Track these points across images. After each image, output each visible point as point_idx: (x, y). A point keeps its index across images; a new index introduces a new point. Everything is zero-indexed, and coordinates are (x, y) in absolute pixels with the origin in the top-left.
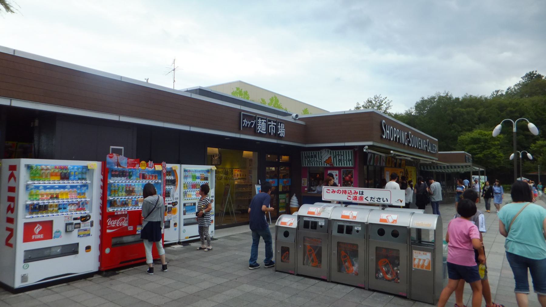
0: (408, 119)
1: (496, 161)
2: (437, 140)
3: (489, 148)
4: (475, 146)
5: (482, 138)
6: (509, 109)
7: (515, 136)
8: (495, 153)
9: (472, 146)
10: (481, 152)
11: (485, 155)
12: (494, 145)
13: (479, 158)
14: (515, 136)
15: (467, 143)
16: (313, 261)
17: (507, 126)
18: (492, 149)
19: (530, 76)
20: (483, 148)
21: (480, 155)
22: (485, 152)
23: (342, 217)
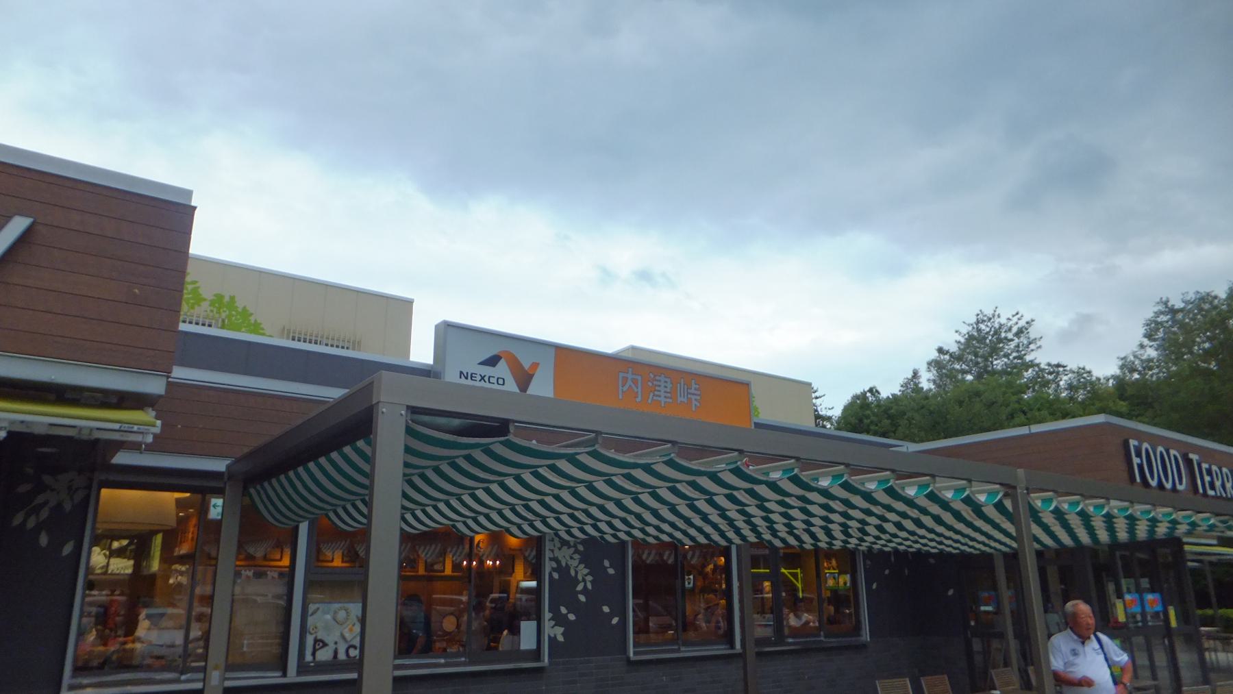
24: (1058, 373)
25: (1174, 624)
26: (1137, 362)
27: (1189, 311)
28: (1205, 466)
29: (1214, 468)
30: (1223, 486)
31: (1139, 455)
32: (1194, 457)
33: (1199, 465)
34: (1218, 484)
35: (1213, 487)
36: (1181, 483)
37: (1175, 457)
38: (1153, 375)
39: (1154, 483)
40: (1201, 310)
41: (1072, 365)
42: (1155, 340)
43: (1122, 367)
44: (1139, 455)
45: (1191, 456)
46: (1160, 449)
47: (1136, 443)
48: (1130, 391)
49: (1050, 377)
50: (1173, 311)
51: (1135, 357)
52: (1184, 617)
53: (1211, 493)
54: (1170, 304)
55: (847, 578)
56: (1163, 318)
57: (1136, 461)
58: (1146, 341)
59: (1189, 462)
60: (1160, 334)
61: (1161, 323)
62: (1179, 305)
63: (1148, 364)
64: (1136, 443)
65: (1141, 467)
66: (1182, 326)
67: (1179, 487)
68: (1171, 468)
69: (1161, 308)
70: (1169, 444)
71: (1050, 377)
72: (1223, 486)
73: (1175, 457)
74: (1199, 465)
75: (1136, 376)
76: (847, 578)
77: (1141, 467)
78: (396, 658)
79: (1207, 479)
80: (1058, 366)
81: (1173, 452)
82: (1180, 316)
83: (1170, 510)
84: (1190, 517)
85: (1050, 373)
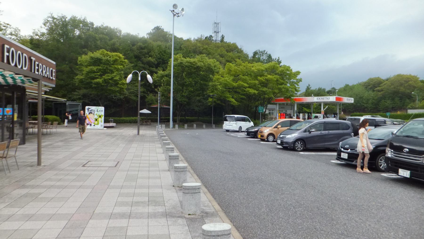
0: (34, 44)
1: (118, 89)
2: (54, 63)
3: (112, 72)
4: (95, 68)
5: (104, 58)
6: (139, 44)
7: (139, 82)
8: (117, 78)
9: (91, 67)
10: (101, 76)
11: (105, 80)
12: (118, 70)
13: (98, 83)
14: (139, 82)
15: (86, 64)
16: (215, 102)
17: (135, 75)
18: (115, 74)
19: (157, 29)
20: (104, 72)
21: (99, 80)
22: (105, 77)
23: (336, 100)
24: (7, 27)
25: (15, 119)
26: (39, 32)
27: (58, 20)
28: (37, 63)
29: (40, 64)
30: (42, 71)
31: (8, 52)
32: (33, 59)
33: (35, 62)
34: (40, 70)
35: (38, 71)
36: (25, 67)
37: (25, 57)
38: (44, 39)
39: (13, 65)
40: (62, 20)
41: (14, 25)
42: (46, 26)
43: (33, 33)
44: (8, 52)
45: (32, 58)
46: (19, 52)
47: (8, 47)
48: (34, 42)
49: (4, 28)
50: (54, 18)
51: (39, 30)
52: (20, 116)
53: (36, 73)
54: (53, 15)
55: (280, 143)
56: (50, 19)
57: (6, 54)
58: (43, 26)
59: (31, 60)
60: (48, 24)
61: (49, 21)
62: (56, 16)
63: (43, 34)
64: (8, 47)
65: (8, 57)
66: (55, 24)
67: (24, 68)
68: (22, 61)
69: (50, 15)
70: (23, 51)
71: (4, 28)
72: (42, 71)
73: (25, 57)
74: (35, 62)
75: (37, 37)
76: (280, 143)
77: (8, 57)
78: (169, 127)
79: (37, 68)
80: (8, 24)
81: (24, 55)
82: (55, 21)
83: (12, 73)
84: (21, 77)
85: (4, 26)
